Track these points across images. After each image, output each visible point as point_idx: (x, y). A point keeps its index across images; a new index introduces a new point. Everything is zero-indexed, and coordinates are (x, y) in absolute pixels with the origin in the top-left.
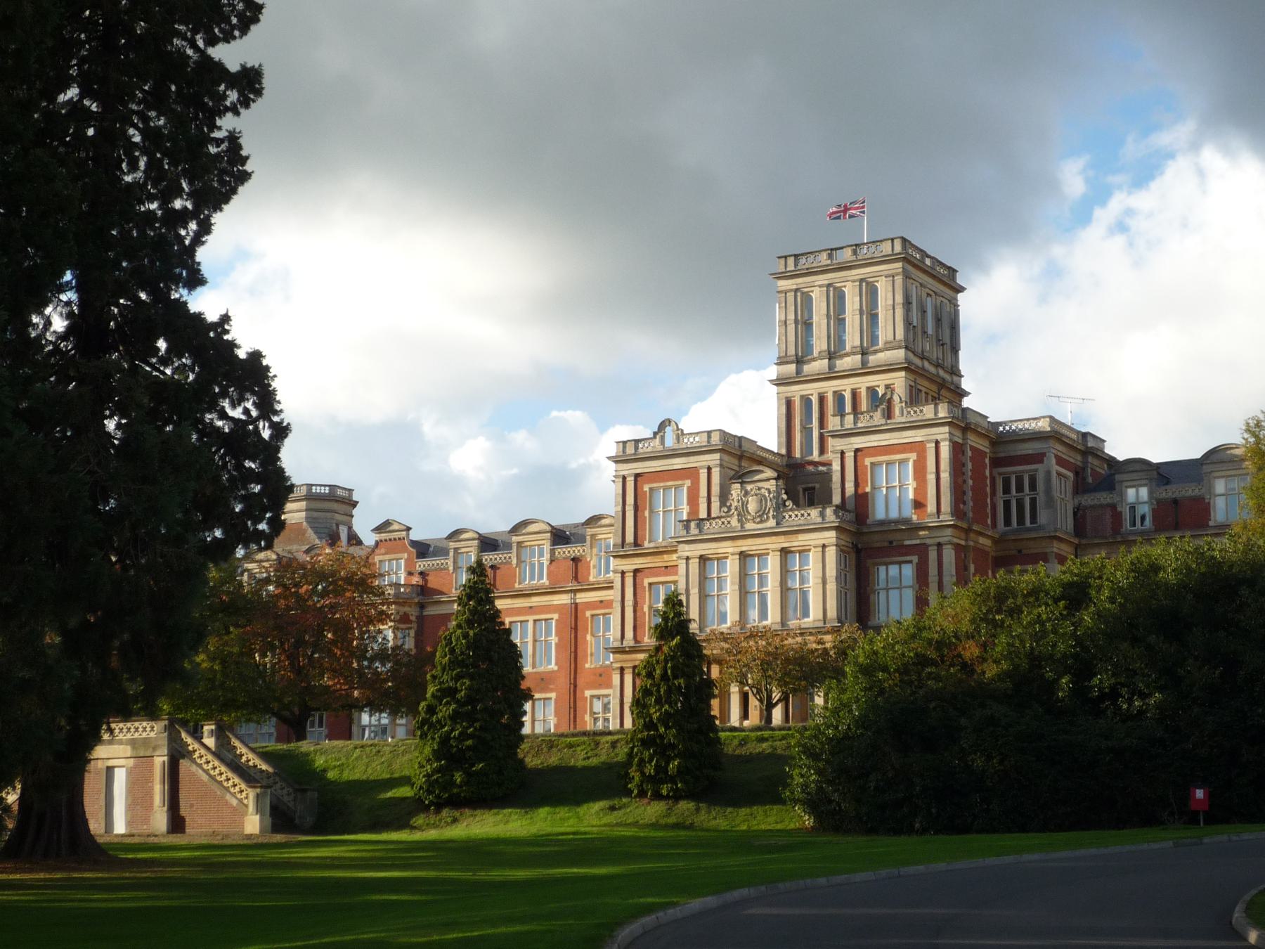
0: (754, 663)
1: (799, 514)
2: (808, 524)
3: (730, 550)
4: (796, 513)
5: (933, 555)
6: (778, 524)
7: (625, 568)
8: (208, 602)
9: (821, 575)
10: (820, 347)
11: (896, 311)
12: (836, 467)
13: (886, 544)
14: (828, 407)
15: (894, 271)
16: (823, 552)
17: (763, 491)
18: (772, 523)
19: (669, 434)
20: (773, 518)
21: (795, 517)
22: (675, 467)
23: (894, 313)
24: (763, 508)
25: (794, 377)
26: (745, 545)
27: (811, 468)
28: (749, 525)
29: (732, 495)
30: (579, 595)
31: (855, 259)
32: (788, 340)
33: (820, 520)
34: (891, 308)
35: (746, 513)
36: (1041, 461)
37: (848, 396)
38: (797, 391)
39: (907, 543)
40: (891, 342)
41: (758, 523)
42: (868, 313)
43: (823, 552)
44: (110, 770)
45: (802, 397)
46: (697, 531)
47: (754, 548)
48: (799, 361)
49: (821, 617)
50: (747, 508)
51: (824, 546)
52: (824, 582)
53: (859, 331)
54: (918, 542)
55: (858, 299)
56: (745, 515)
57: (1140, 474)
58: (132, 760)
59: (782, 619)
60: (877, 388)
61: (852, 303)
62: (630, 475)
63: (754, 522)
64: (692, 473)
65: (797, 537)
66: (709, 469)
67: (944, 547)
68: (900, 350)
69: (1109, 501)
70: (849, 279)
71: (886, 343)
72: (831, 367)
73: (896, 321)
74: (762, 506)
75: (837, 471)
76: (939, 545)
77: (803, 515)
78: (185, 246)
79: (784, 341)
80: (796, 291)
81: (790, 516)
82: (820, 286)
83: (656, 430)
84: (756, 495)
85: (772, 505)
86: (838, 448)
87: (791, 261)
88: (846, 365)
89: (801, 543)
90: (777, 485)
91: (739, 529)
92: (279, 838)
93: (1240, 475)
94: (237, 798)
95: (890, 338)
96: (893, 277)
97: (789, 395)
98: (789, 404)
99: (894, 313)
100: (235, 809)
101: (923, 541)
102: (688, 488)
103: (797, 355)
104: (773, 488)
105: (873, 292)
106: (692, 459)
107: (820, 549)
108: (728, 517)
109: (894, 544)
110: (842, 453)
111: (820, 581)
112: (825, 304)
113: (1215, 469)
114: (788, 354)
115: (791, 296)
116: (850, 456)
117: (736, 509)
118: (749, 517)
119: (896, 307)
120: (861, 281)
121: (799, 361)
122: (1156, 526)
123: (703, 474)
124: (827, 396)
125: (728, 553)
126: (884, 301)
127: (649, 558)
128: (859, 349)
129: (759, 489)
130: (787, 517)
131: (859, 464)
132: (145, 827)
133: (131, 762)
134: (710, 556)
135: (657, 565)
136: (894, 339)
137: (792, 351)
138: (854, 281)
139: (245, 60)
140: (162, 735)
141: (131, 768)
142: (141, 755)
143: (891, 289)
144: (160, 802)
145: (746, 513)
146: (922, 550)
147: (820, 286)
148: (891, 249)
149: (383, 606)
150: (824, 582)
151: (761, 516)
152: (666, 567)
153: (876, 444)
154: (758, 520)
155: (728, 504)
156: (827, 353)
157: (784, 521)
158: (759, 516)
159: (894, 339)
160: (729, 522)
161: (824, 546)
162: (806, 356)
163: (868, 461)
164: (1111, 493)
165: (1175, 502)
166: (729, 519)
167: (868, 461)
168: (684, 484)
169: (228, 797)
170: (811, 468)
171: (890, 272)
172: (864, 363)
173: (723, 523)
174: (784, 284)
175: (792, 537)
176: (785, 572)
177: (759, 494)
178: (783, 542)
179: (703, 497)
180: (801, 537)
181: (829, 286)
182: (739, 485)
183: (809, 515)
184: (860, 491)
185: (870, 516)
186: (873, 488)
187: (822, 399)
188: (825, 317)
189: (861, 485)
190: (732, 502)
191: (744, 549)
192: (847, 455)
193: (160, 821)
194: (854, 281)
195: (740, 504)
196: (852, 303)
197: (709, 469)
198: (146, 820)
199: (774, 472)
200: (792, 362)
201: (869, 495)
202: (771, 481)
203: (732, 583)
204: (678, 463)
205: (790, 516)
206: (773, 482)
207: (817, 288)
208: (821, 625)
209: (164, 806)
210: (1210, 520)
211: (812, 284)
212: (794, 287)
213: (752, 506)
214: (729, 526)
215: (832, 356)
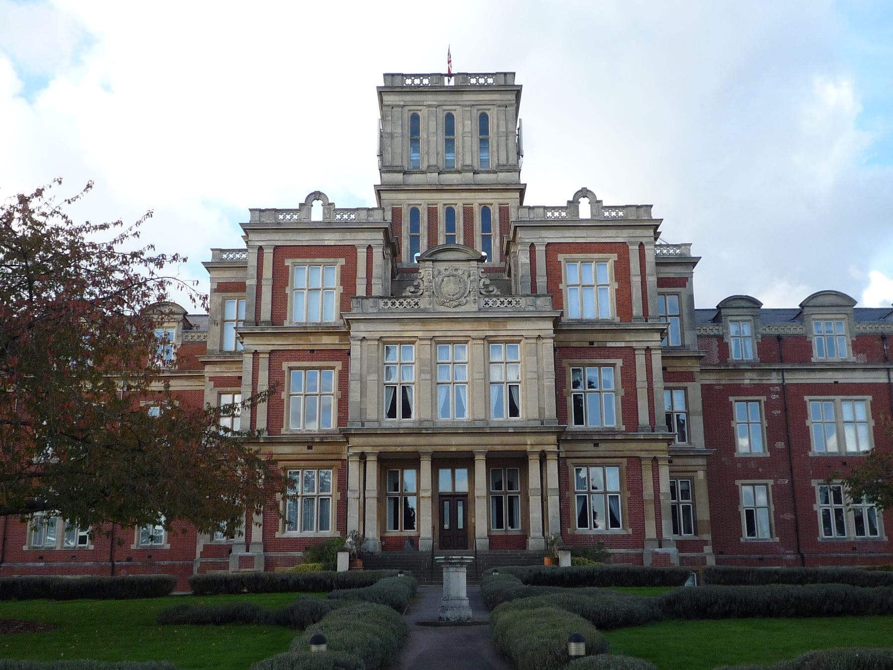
0: (131, 461)
1: (506, 301)
4: (502, 299)
5: (640, 359)
7: (259, 348)
10: (428, 161)
13: (587, 345)
15: (508, 102)
19: (317, 206)
22: (326, 243)
30: (172, 383)
36: (684, 286)
37: (459, 211)
39: (609, 345)
54: (623, 344)
57: (745, 310)
62: (268, 246)
64: (349, 252)
65: (506, 326)
66: (369, 248)
67: (652, 352)
69: (716, 332)
70: (460, 103)
76: (648, 350)
77: (510, 303)
83: (303, 202)
89: (510, 333)
93: (825, 319)
101: (629, 345)
106: (348, 236)
108: (416, 297)
109: (596, 345)
113: (815, 312)
116: (540, 250)
122: (761, 358)
123: (362, 255)
127: (291, 338)
129: (456, 270)
135: (301, 348)
146: (628, 354)
149: (141, 288)
152: (312, 351)
160: (417, 304)
164: (718, 326)
165: (779, 338)
166: (416, 300)
171: (503, 103)
180: (511, 326)
183: (518, 303)
190: (420, 281)
197: (369, 248)
204: (330, 239)
210: (812, 356)
214: (416, 307)
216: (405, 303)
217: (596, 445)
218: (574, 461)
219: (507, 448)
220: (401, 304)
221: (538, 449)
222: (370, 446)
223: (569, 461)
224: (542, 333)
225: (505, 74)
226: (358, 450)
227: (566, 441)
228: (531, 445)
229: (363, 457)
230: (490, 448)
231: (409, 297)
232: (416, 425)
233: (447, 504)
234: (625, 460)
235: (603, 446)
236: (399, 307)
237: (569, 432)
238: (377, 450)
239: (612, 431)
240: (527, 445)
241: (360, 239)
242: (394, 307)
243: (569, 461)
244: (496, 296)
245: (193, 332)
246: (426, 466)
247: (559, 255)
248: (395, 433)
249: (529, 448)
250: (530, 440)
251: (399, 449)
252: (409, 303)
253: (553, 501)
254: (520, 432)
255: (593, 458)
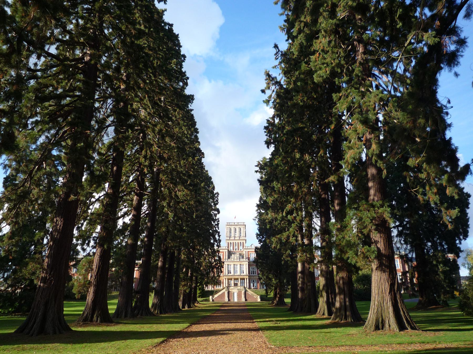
18: (238, 260)
21: (242, 260)
26: (234, 263)
38: (229, 241)
61: (238, 230)
78: (383, 179)
123: (225, 253)
139: (454, 125)
151: (237, 259)
155: (373, 241)
176: (240, 268)
187: (233, 243)
193: (243, 299)
196: (238, 230)
198: (241, 299)
207: (232, 228)
213: (236, 258)
215: (235, 237)
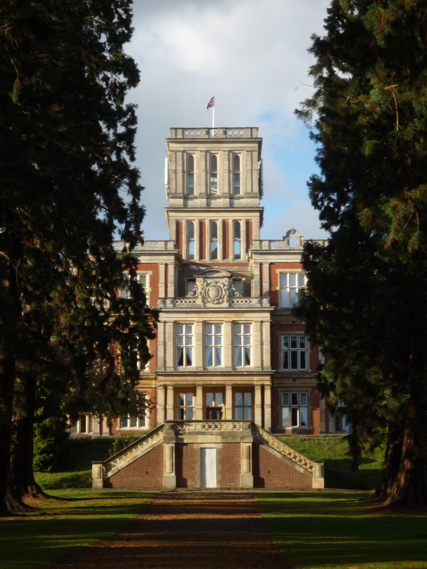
1: (244, 301)
2: (251, 308)
3: (196, 319)
4: (242, 299)
6: (230, 306)
8: (138, 345)
9: (260, 339)
11: (253, 174)
12: (257, 272)
13: (291, 323)
14: (205, 229)
16: (261, 326)
17: (219, 284)
18: (225, 305)
20: (227, 302)
23: (252, 175)
24: (220, 295)
25: (181, 208)
26: (207, 317)
27: (195, 267)
28: (209, 305)
29: (196, 284)
31: (225, 137)
32: (178, 183)
33: (259, 305)
34: (250, 171)
35: (207, 297)
37: (219, 224)
38: (184, 217)
40: (249, 193)
41: (216, 304)
42: (233, 173)
43: (261, 326)
44: (203, 450)
45: (187, 221)
46: (171, 306)
47: (213, 319)
48: (186, 198)
49: (259, 365)
50: (208, 294)
51: (262, 322)
52: (262, 344)
53: (228, 184)
55: (227, 163)
56: (207, 298)
58: (221, 444)
59: (232, 365)
60: (239, 221)
63: (213, 303)
65: (243, 315)
66: (166, 265)
68: (256, 199)
70: (221, 149)
71: (246, 193)
72: (208, 204)
73: (253, 181)
74: (219, 293)
75: (257, 275)
79: (175, 183)
80: (184, 152)
81: (238, 302)
82: (201, 151)
84: (215, 286)
85: (226, 293)
86: (258, 261)
87: (180, 132)
88: (218, 204)
90: (229, 281)
91: (203, 306)
92: (329, 491)
94: (303, 468)
95: (249, 190)
96: (252, 152)
97: (178, 218)
98: (178, 224)
99: (252, 175)
100: (302, 474)
102: (151, 276)
103: (183, 193)
104: (227, 283)
105: (236, 159)
106: (154, 257)
107: (259, 323)
108: (194, 298)
110: (261, 264)
111: (259, 343)
112: (204, 163)
114: (178, 192)
115: (179, 155)
117: (201, 294)
118: (209, 300)
119: (253, 171)
120: (230, 151)
121: (186, 198)
123: (162, 269)
124: (205, 222)
125: (194, 321)
126: (244, 166)
128: (228, 195)
129: (216, 283)
130: (235, 301)
131: (272, 272)
132: (232, 484)
133: (221, 446)
134: (181, 322)
136: (252, 191)
137: (180, 190)
138: (224, 151)
140: (247, 430)
141: (220, 449)
142: (230, 442)
143: (250, 159)
144: (247, 469)
145: (207, 297)
147: (201, 151)
148: (250, 134)
150: (262, 344)
151: (219, 299)
153: (284, 261)
154: (216, 302)
156: (205, 194)
157: (234, 304)
158: (217, 300)
159: (252, 191)
160: (194, 302)
161: (262, 322)
162: (190, 195)
163: (278, 271)
166: (194, 300)
167: (278, 271)
168: (147, 273)
169: (297, 467)
170: (195, 267)
172: (231, 205)
173: (190, 302)
174: (174, 146)
175: (240, 315)
177: (216, 286)
178: (233, 317)
179: (162, 283)
180: (246, 315)
181: (207, 151)
182: (202, 279)
183: (250, 302)
184: (273, 289)
185: (279, 304)
186: (281, 288)
188: (204, 171)
189: (273, 285)
190: (196, 289)
191: (206, 319)
192: (264, 266)
194: (224, 151)
195: (204, 291)
197: (166, 265)
199: (228, 273)
200: (180, 198)
201: (279, 292)
202: (225, 278)
203: (197, 340)
205: (238, 302)
206: (227, 279)
208: (260, 370)
209: (250, 471)
211: (195, 149)
212: (182, 149)
213: (212, 293)
214: (194, 304)
215: (209, 196)
216: (188, 301)
217: (294, 380)
218: (282, 389)
219: (243, 382)
220: (186, 302)
221: (260, 383)
222: (170, 381)
223: (279, 389)
224: (263, 319)
225: (251, 128)
226: (163, 383)
227: (278, 378)
228: (257, 381)
229: (165, 388)
230: (234, 382)
231: (190, 298)
232: (195, 370)
233: (211, 412)
234: (310, 389)
235: (298, 381)
236: (182, 304)
237: (279, 373)
238: (173, 383)
239: (303, 373)
240: (254, 381)
241: (161, 260)
242: (181, 304)
243: (279, 389)
244: (238, 298)
245: (217, 421)
246: (199, 392)
247: (277, 270)
248: (183, 375)
249: (255, 383)
250: (256, 378)
251: (185, 383)
252: (190, 302)
253: (268, 411)
254: (250, 374)
255: (293, 387)
